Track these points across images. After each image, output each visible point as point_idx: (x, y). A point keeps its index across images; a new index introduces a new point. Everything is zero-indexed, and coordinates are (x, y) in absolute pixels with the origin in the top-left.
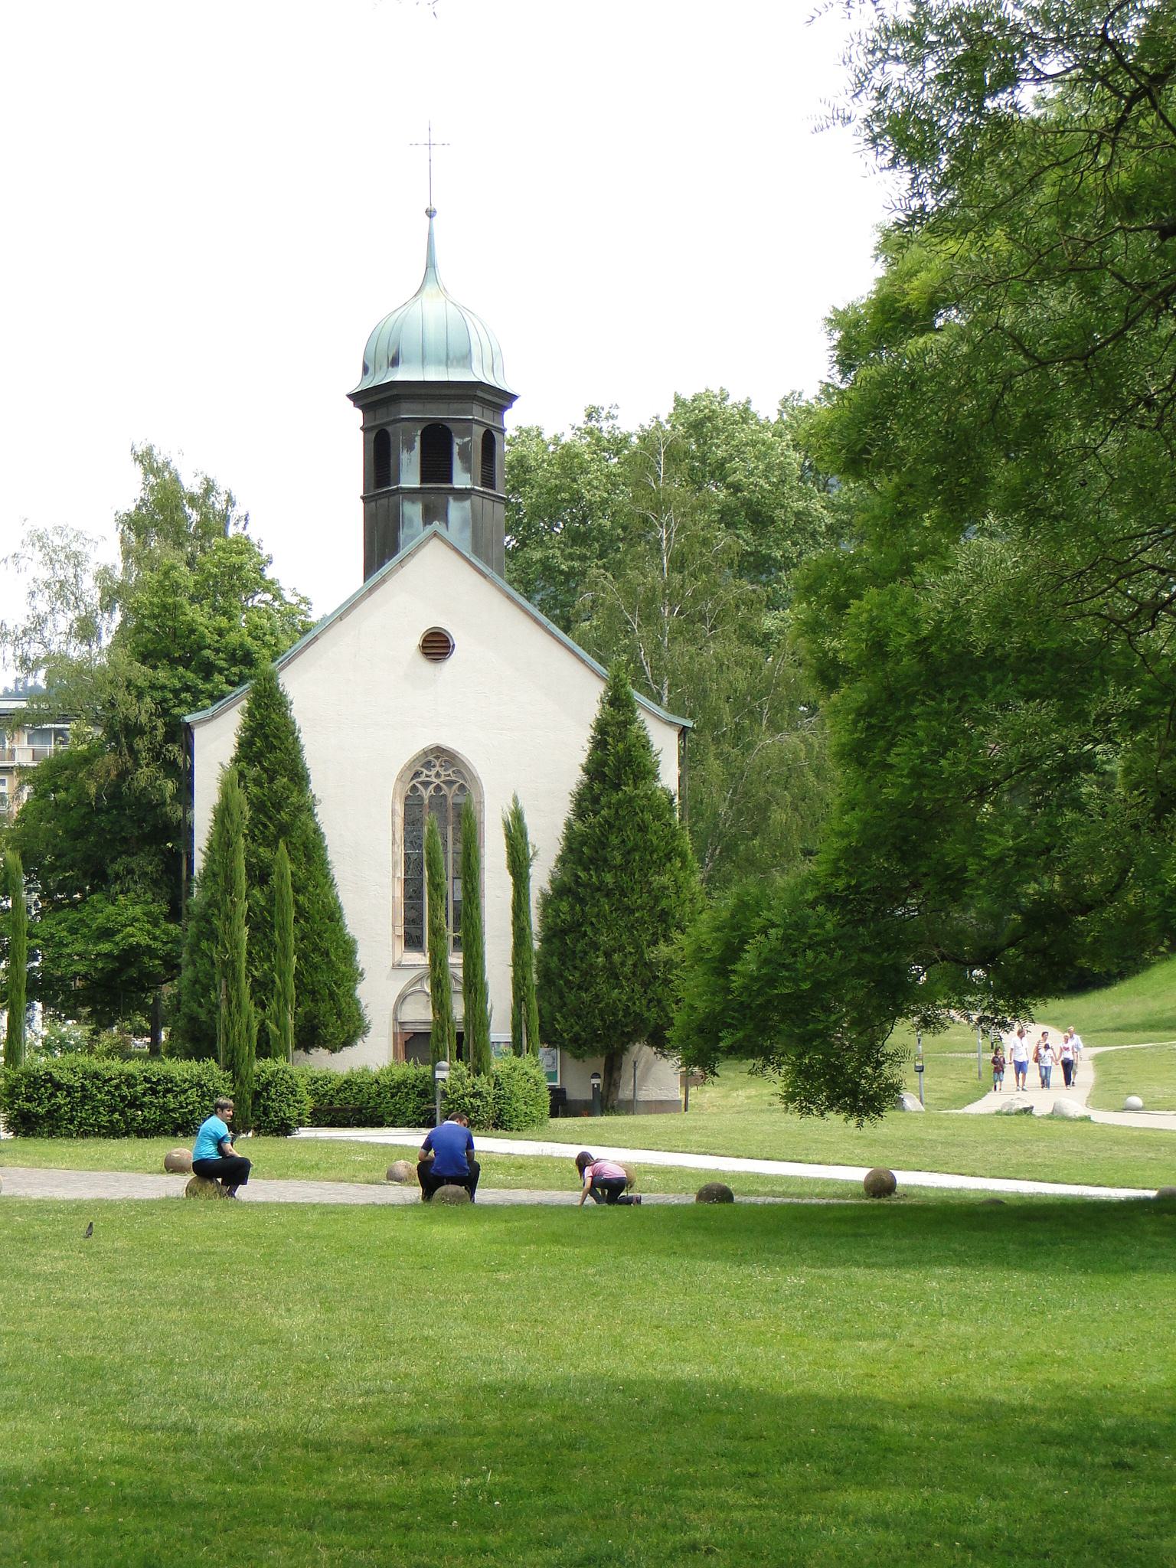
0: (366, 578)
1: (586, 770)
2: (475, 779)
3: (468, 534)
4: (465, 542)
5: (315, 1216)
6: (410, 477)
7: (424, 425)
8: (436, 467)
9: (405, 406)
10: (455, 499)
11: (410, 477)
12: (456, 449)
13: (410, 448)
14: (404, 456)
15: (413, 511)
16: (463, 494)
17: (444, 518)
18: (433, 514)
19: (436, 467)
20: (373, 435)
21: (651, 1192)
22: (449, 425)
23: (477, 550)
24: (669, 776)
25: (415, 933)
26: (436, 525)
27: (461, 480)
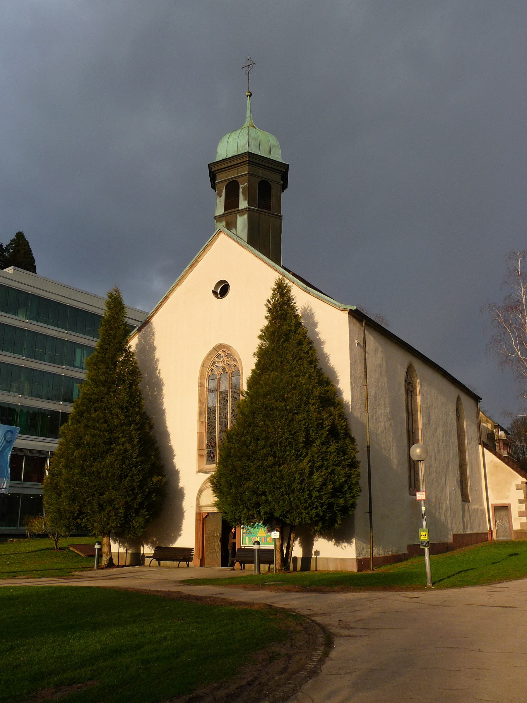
7: (226, 183)
10: (240, 216)
16: (242, 212)
27: (243, 204)
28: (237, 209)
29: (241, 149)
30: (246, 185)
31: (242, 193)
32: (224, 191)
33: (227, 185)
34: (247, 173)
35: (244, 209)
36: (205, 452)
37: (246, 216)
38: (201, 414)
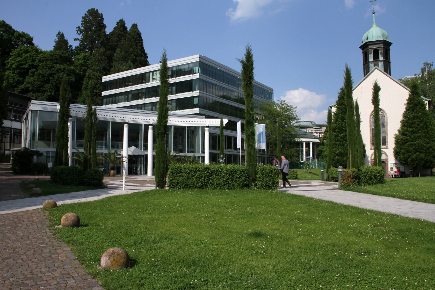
0: (364, 76)
1: (395, 144)
2: (386, 113)
3: (383, 68)
4: (382, 69)
5: (155, 144)
6: (371, 58)
7: (373, 49)
8: (376, 57)
9: (369, 46)
11: (371, 58)
13: (371, 54)
14: (370, 55)
15: (371, 65)
16: (381, 61)
17: (378, 66)
18: (376, 65)
19: (376, 57)
20: (364, 53)
21: (221, 87)
22: (378, 49)
23: (385, 71)
24: (428, 109)
25: (384, 142)
26: (376, 67)
27: (381, 58)
36: (372, 143)
37: (382, 63)
38: (371, 130)
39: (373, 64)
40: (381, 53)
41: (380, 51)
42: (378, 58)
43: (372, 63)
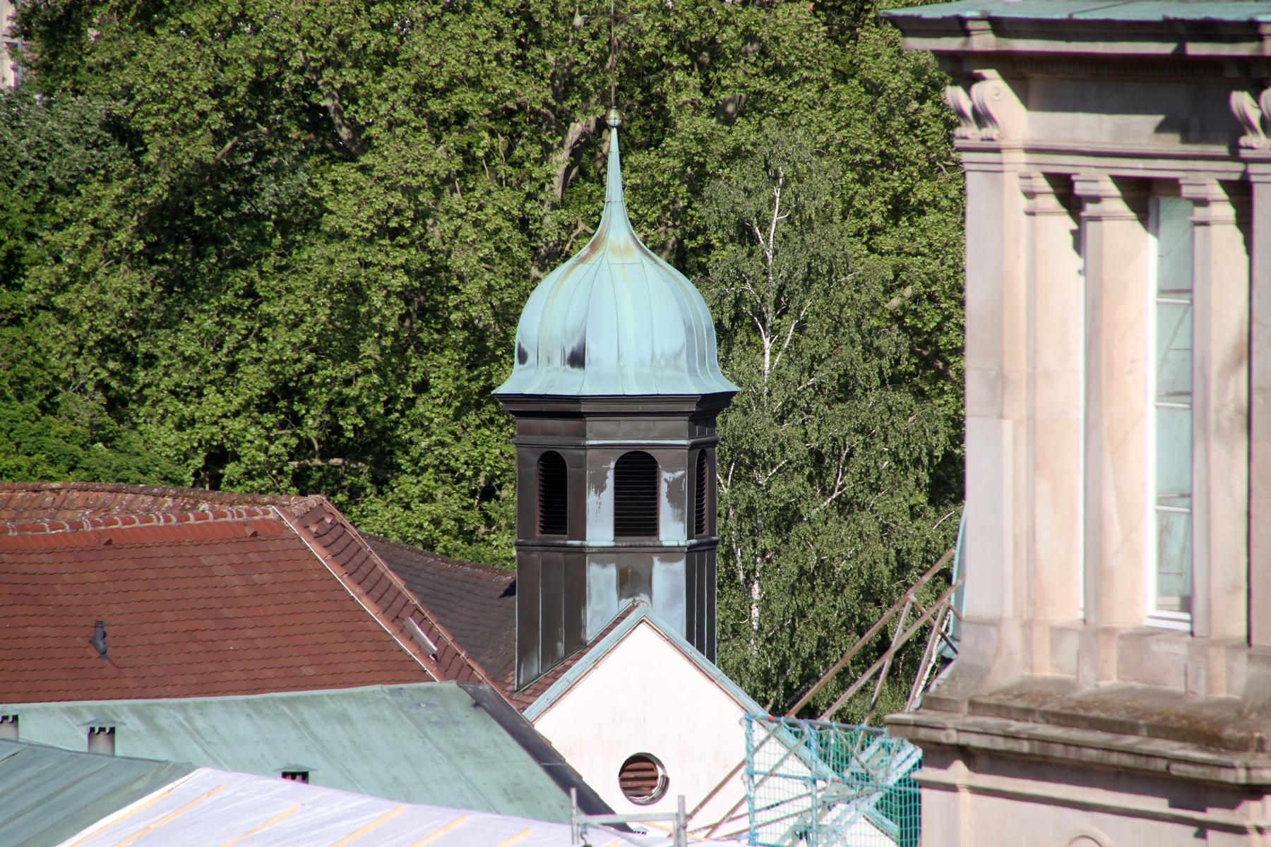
10: (663, 560)
12: (663, 488)
13: (600, 488)
14: (591, 499)
16: (669, 553)
28: (646, 541)
29: (663, 362)
30: (683, 476)
31: (669, 495)
32: (611, 475)
33: (622, 458)
34: (684, 442)
35: (679, 546)
37: (680, 566)
39: (612, 571)
40: (673, 486)
41: (666, 477)
42: (650, 527)
43: (604, 564)
